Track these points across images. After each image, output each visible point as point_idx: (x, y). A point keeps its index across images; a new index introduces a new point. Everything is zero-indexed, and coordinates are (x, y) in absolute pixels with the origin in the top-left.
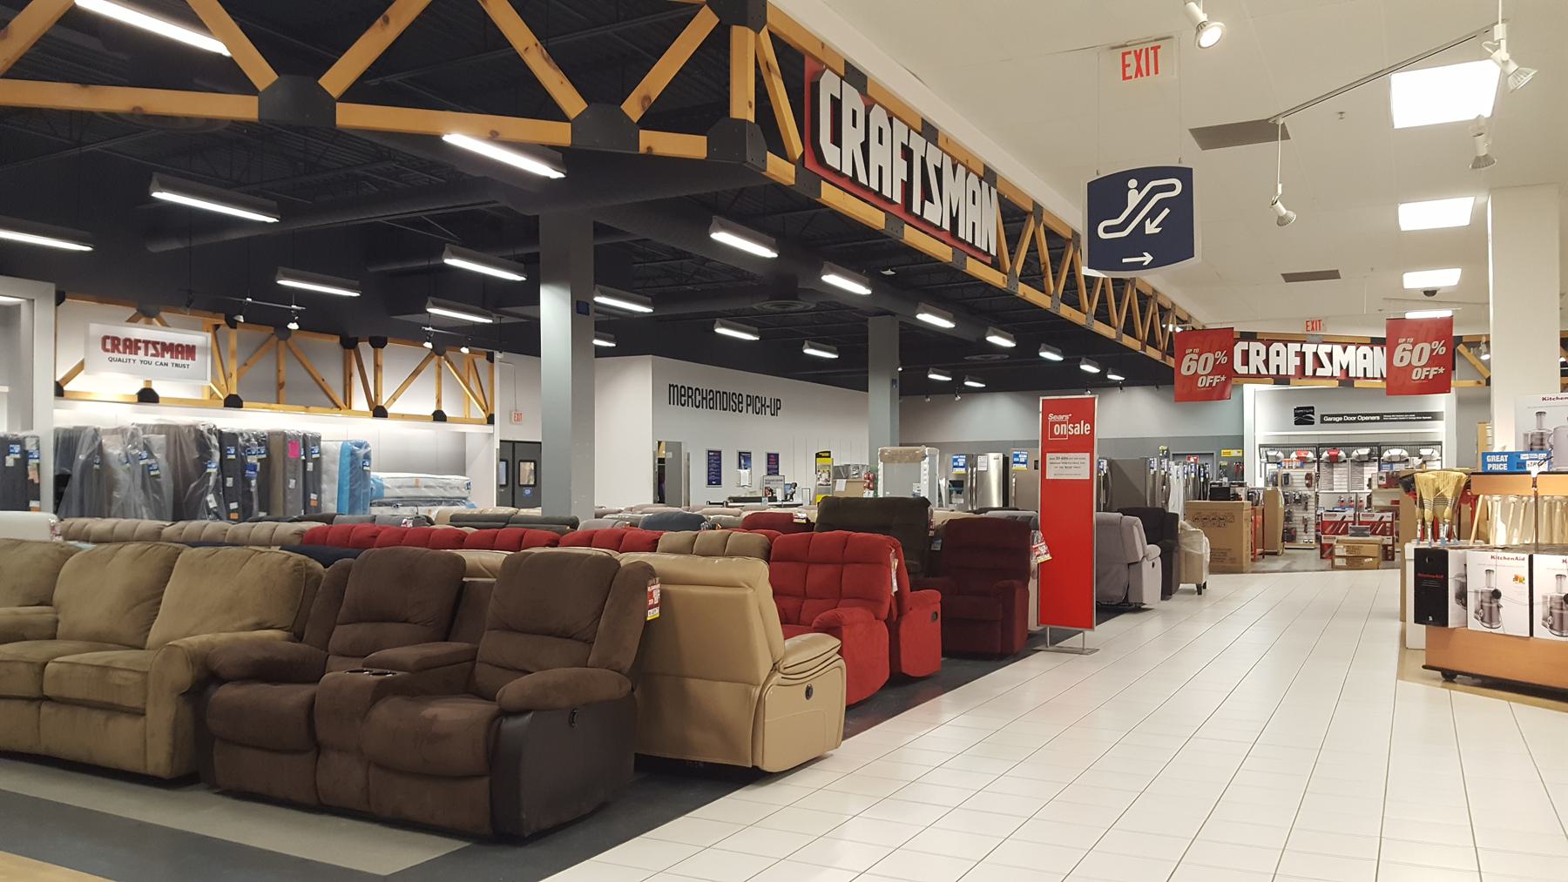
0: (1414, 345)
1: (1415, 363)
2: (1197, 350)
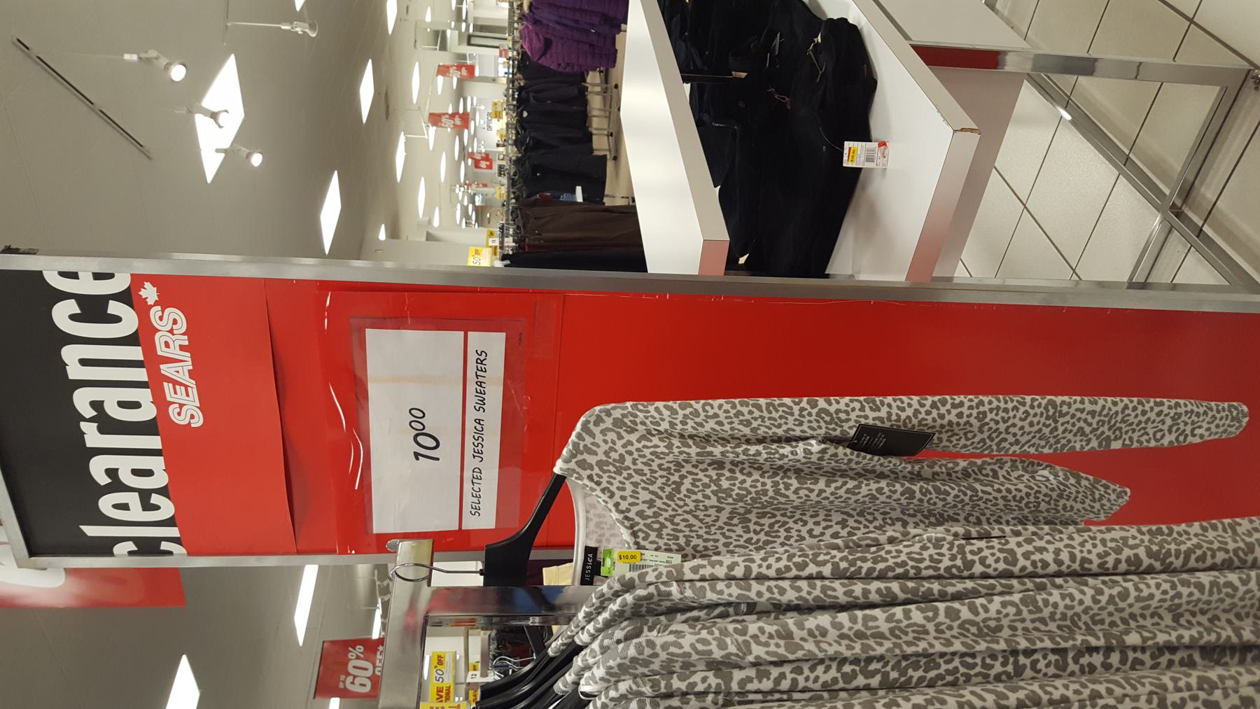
0: (348, 674)
1: (369, 673)
2: (342, 677)
